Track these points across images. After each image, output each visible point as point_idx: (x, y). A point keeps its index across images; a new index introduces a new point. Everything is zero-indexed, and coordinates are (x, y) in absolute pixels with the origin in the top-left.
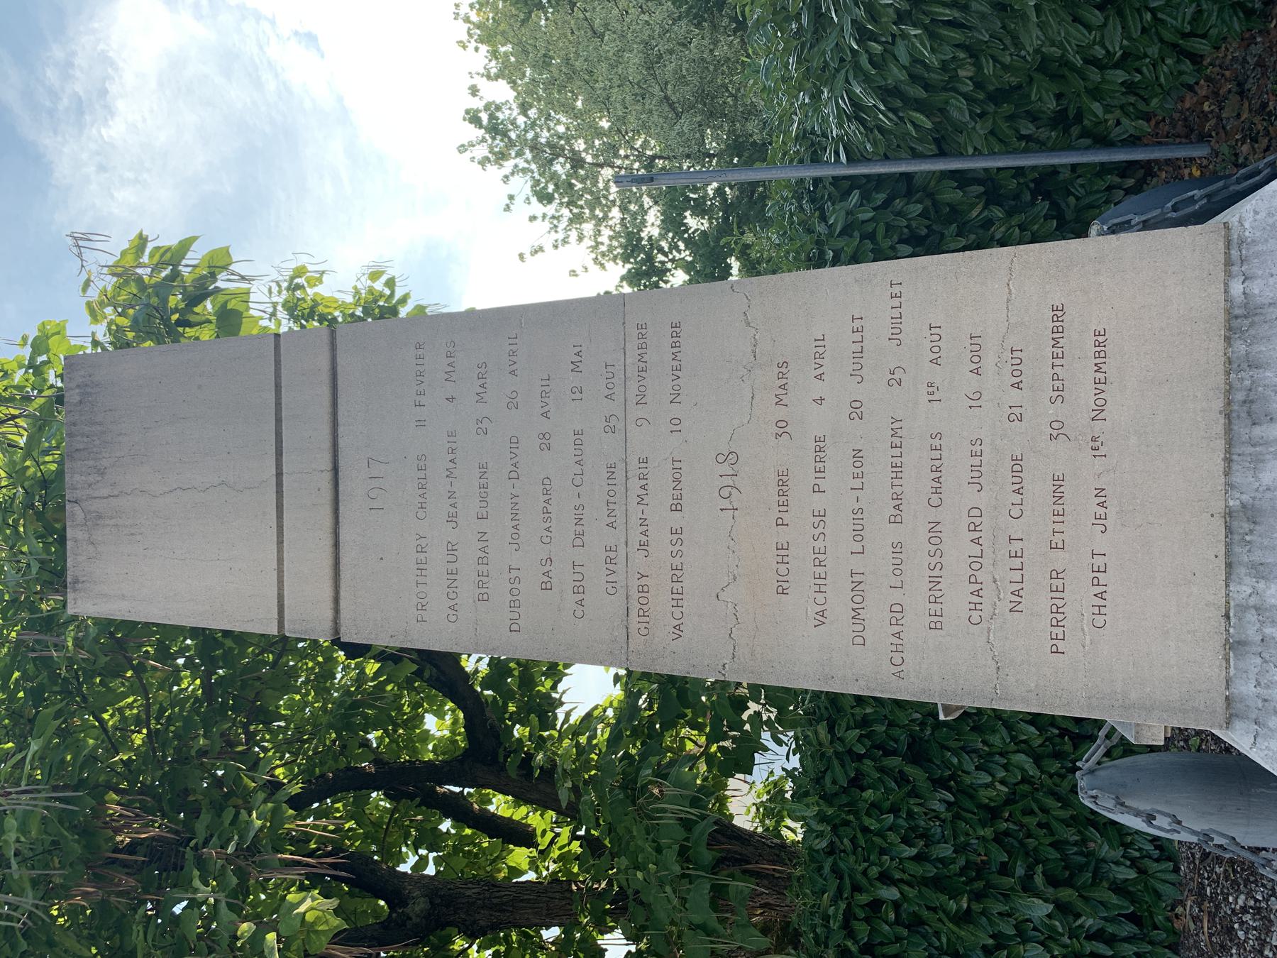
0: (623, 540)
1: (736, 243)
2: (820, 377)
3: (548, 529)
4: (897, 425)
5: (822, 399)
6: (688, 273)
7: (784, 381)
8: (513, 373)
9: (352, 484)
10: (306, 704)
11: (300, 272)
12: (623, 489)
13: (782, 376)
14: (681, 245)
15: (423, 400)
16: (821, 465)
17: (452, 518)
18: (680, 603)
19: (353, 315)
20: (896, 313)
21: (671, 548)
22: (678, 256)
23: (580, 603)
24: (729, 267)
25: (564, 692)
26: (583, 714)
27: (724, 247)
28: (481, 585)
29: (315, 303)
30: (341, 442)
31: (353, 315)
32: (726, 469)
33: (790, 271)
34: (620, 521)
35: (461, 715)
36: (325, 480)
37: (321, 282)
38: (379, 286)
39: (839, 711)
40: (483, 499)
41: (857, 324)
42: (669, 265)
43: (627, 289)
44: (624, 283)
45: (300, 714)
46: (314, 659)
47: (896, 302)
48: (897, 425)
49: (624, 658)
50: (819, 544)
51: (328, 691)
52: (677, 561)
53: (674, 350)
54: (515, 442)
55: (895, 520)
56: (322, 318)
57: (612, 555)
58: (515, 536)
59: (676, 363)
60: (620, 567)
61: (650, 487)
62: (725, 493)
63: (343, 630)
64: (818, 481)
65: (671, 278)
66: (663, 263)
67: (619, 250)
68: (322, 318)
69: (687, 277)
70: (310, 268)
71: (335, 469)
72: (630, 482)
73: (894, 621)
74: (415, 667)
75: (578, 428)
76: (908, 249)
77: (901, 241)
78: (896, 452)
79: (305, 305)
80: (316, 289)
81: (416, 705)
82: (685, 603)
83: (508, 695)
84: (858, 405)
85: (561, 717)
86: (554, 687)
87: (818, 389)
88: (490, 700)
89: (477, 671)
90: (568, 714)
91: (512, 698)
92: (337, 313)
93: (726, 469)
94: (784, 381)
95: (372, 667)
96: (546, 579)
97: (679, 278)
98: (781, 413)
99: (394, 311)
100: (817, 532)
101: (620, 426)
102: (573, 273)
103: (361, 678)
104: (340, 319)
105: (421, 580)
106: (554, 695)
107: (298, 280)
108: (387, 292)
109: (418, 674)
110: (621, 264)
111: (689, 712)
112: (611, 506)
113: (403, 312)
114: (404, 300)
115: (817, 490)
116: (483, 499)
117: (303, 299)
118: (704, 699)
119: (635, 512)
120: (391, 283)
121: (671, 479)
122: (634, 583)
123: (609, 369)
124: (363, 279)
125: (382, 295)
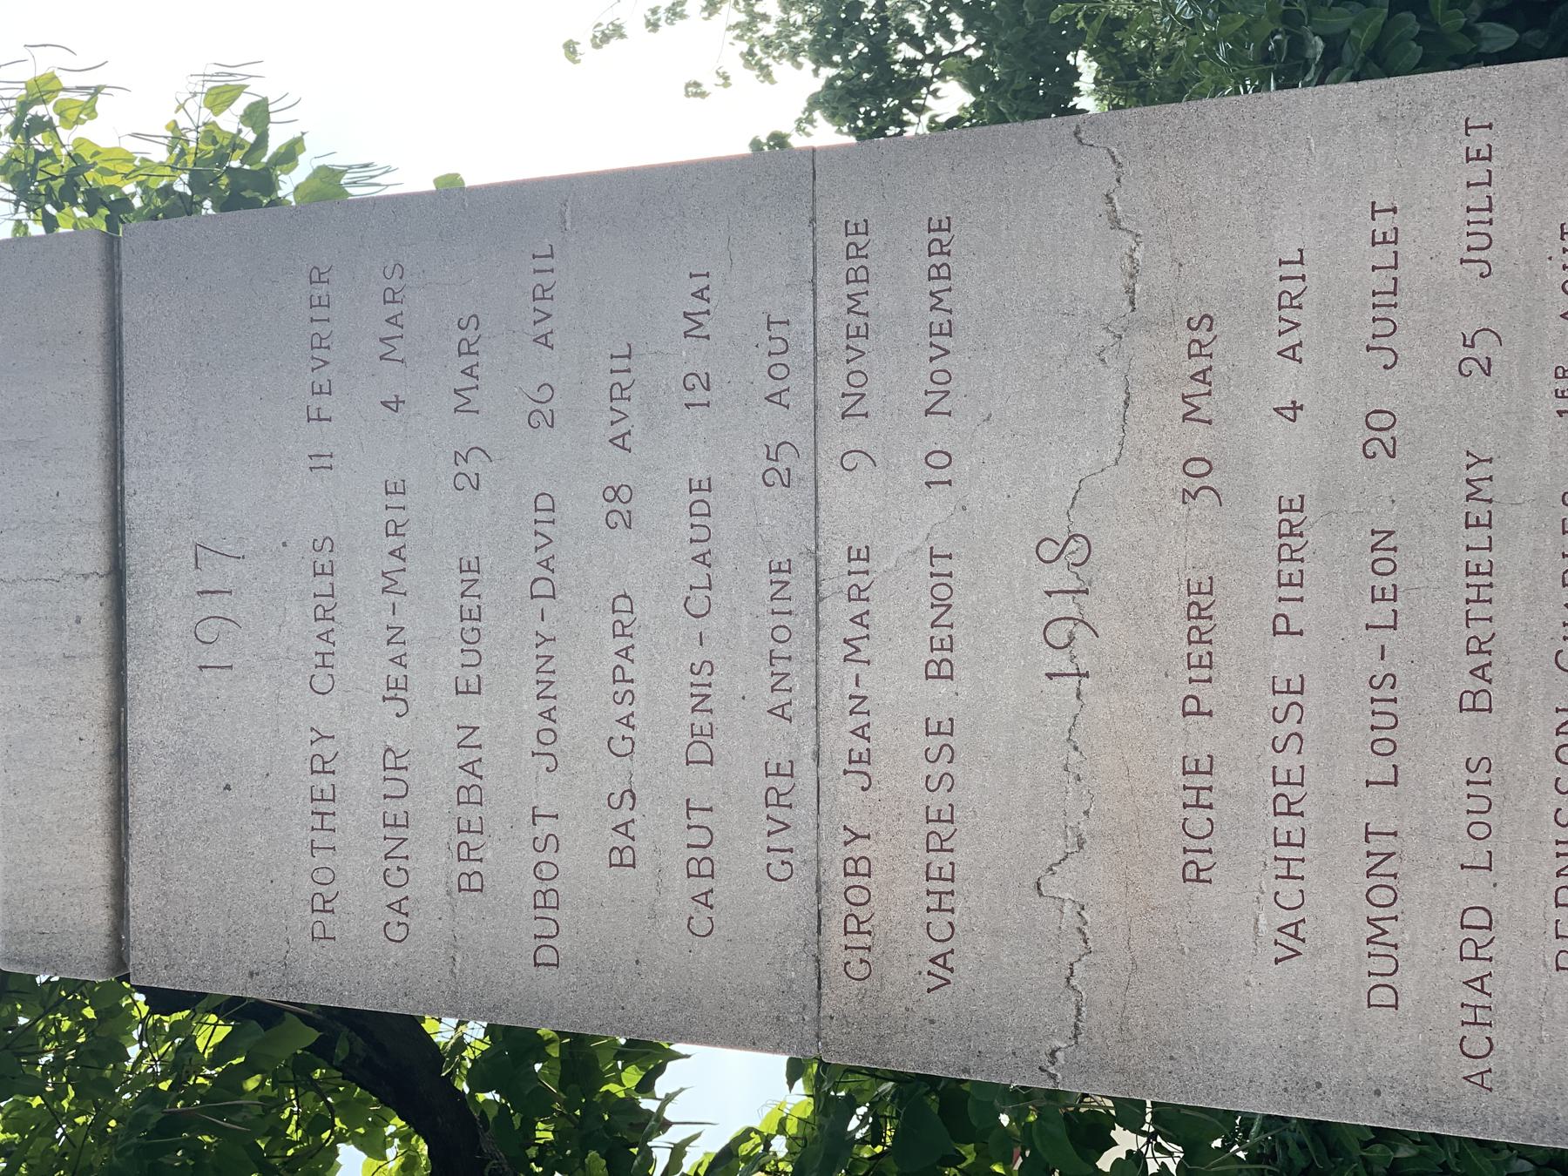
0: (808, 748)
1: (1088, 18)
2: (1291, 353)
3: (627, 721)
4: (1479, 471)
5: (1295, 407)
6: (972, 87)
7: (1204, 363)
8: (543, 340)
9: (160, 607)
10: (57, 1117)
11: (41, 89)
12: (809, 625)
13: (1197, 349)
14: (957, 22)
15: (327, 404)
16: (1294, 567)
17: (396, 692)
18: (947, 902)
19: (167, 191)
20: (1478, 198)
21: (927, 769)
22: (947, 47)
23: (704, 900)
24: (1075, 74)
25: (669, 1098)
26: (717, 1148)
27: (1060, 25)
28: (465, 853)
29: (79, 166)
30: (132, 508)
31: (167, 191)
32: (1059, 576)
33: (1218, 90)
34: (802, 702)
35: (423, 1148)
36: (91, 600)
37: (92, 114)
38: (229, 121)
39: (1332, 1154)
40: (470, 646)
41: (1384, 223)
42: (926, 70)
43: (826, 134)
44: (817, 114)
45: (42, 1143)
46: (74, 1011)
47: (1478, 172)
48: (1479, 471)
49: (809, 1032)
50: (1288, 761)
51: (107, 1087)
52: (939, 800)
53: (936, 286)
54: (546, 508)
55: (1474, 705)
56: (94, 201)
57: (783, 784)
58: (547, 737)
59: (939, 317)
60: (802, 815)
61: (876, 619)
62: (1059, 634)
63: (135, 956)
64: (1285, 608)
65: (930, 101)
66: (911, 64)
67: (806, 34)
68: (94, 201)
69: (969, 99)
70: (67, 80)
71: (117, 572)
72: (826, 606)
73: (1469, 950)
74: (312, 1035)
75: (700, 474)
76: (1500, 35)
77: (1488, 16)
78: (1478, 537)
79: (54, 170)
80: (81, 131)
81: (314, 1125)
82: (958, 903)
83: (533, 1103)
84: (1385, 420)
85: (662, 1158)
86: (646, 1087)
87: (1287, 382)
88: (492, 1114)
89: (460, 1045)
90: (678, 1151)
91: (545, 1113)
92: (129, 188)
93: (1059, 576)
94: (1204, 363)
95: (211, 1033)
96: (621, 841)
97: (951, 98)
98: (1198, 439)
99: (265, 181)
100: (1282, 731)
101: (802, 469)
102: (695, 89)
103: (184, 1060)
104: (137, 203)
105: (321, 839)
106: (647, 1104)
107: (38, 110)
108: (249, 136)
109: (322, 1051)
110: (808, 65)
111: (969, 1152)
112: (780, 666)
113: (288, 184)
114: (289, 155)
115: (1283, 628)
116: (469, 646)
117: (50, 154)
118: (1004, 1119)
119: (840, 680)
120: (258, 115)
121: (927, 600)
122: (835, 854)
123: (777, 330)
124: (192, 106)
125: (235, 143)
